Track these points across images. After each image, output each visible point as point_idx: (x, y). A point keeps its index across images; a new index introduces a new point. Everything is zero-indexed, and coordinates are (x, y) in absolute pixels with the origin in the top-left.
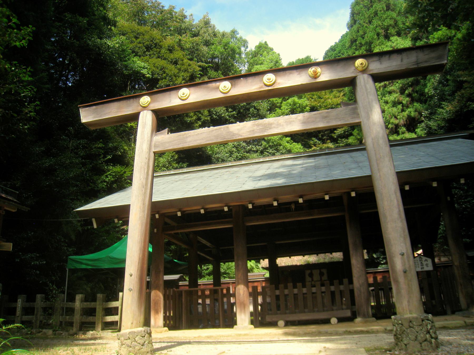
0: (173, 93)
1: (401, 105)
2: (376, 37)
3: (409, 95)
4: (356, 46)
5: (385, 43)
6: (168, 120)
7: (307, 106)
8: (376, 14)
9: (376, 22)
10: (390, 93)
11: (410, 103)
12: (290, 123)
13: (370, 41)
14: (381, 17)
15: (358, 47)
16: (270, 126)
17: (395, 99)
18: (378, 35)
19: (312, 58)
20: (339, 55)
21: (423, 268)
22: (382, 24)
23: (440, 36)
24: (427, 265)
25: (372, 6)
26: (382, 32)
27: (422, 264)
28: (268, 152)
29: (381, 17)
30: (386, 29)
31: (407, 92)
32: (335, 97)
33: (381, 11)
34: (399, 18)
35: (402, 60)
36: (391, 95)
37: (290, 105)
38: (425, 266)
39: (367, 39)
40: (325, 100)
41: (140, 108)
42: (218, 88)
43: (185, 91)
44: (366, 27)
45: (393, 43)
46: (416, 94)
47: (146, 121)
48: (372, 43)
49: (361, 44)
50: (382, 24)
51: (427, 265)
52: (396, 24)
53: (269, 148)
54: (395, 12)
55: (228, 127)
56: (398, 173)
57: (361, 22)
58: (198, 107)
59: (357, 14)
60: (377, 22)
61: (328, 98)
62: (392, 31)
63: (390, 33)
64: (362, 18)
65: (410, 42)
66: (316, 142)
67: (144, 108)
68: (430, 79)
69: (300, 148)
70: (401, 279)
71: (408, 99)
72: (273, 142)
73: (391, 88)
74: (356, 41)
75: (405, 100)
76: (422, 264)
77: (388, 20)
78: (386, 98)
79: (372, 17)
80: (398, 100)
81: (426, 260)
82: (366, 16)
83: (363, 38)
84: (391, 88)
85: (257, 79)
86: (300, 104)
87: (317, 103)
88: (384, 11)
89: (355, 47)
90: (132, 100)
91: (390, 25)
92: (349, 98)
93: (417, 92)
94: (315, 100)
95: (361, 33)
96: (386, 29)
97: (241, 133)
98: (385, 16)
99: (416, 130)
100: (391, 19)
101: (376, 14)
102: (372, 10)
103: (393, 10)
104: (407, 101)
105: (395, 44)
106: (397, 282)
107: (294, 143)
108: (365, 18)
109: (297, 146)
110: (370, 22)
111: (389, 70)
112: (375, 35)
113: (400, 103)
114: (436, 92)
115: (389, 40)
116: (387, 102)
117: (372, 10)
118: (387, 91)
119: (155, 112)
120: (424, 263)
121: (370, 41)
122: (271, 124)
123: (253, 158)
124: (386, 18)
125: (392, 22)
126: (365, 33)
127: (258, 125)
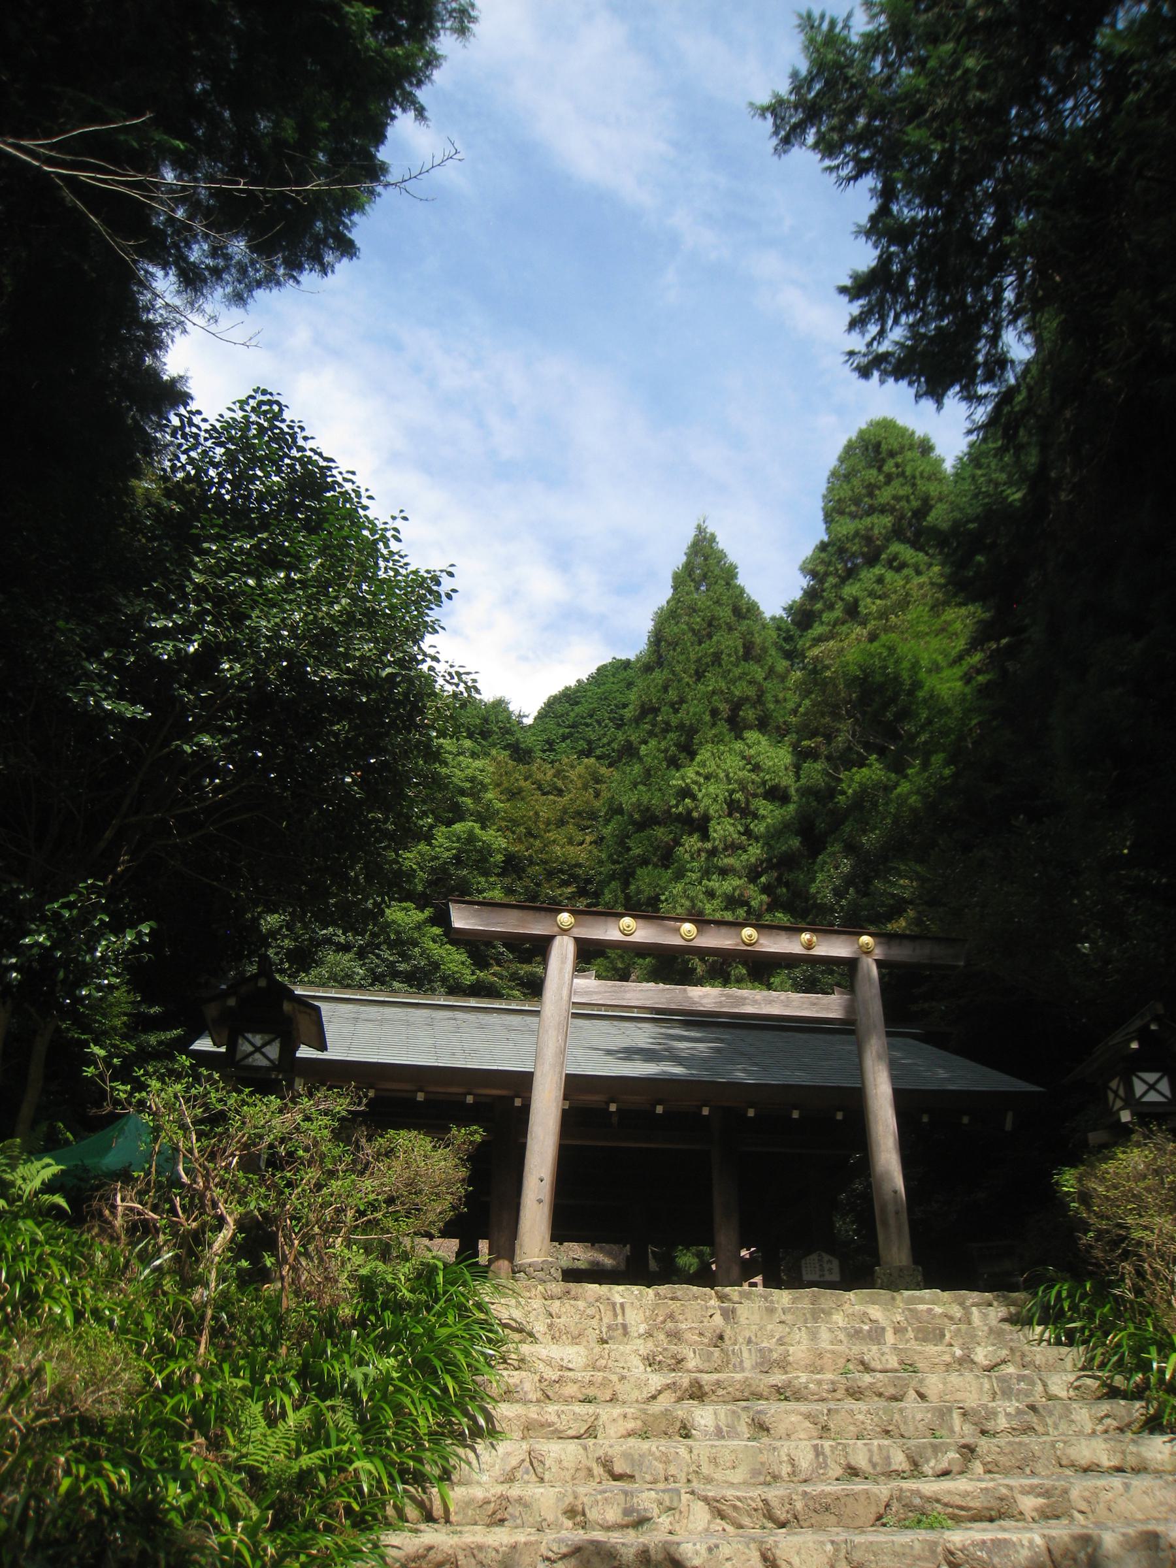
0: (611, 920)
1: (745, 908)
2: (707, 718)
3: (766, 889)
4: (654, 725)
5: (727, 739)
6: (588, 954)
7: (499, 851)
8: (717, 658)
9: (713, 682)
10: (724, 872)
11: (767, 910)
12: (770, 1002)
13: (691, 724)
14: (729, 671)
15: (657, 730)
16: (742, 1001)
17: (734, 890)
18: (714, 713)
19: (511, 707)
20: (589, 721)
21: (823, 1275)
22: (729, 689)
23: (864, 780)
24: (830, 1270)
25: (710, 636)
26: (724, 708)
27: (822, 1270)
28: (378, 956)
29: (729, 671)
30: (736, 706)
31: (763, 879)
32: (570, 842)
33: (729, 655)
34: (767, 685)
35: (914, 950)
36: (724, 879)
37: (459, 839)
38: (826, 1273)
39: (686, 714)
40: (545, 846)
41: (556, 929)
42: (678, 930)
43: (627, 921)
44: (688, 684)
45: (750, 747)
46: (784, 890)
47: (563, 952)
48: (697, 732)
49: (667, 723)
50: (729, 689)
51: (830, 1270)
52: (760, 697)
53: (384, 947)
54: (762, 667)
55: (685, 990)
56: (567, 1075)
57: (678, 669)
58: (642, 950)
59: (669, 644)
60: (716, 682)
61: (554, 841)
62: (749, 714)
63: (744, 719)
64: (681, 658)
65: (789, 756)
66: (502, 954)
67: (564, 932)
68: (825, 862)
69: (463, 963)
70: (892, 1222)
71: (764, 897)
72: (398, 933)
73: (726, 861)
74: (655, 711)
75: (758, 899)
76: (822, 1270)
77: (744, 684)
78: (712, 883)
79: (707, 665)
80: (741, 895)
81: (829, 1261)
82: (693, 657)
83: (676, 711)
84: (726, 861)
85: (733, 931)
86: (484, 842)
87: (523, 848)
88: (737, 658)
89: (648, 727)
90: (543, 913)
91: (747, 699)
92: (610, 856)
93: (787, 885)
94: (520, 840)
95: (672, 695)
96: (736, 706)
97: (704, 1001)
98: (737, 672)
99: (772, 980)
100: (750, 682)
101: (717, 658)
102: (709, 647)
103: (759, 660)
104: (761, 903)
105: (752, 752)
106: (885, 1224)
107: (448, 946)
108: (688, 659)
109: (457, 957)
110: (699, 676)
111: (899, 959)
112: (707, 713)
113: (746, 903)
114: (838, 902)
115: (739, 737)
116: (711, 894)
117: (709, 647)
118: (716, 867)
119: (578, 941)
120: (826, 1266)
121: (691, 724)
122: (745, 998)
123: (509, 998)
124: (740, 678)
125: (751, 692)
126: (682, 701)
127: (728, 996)
